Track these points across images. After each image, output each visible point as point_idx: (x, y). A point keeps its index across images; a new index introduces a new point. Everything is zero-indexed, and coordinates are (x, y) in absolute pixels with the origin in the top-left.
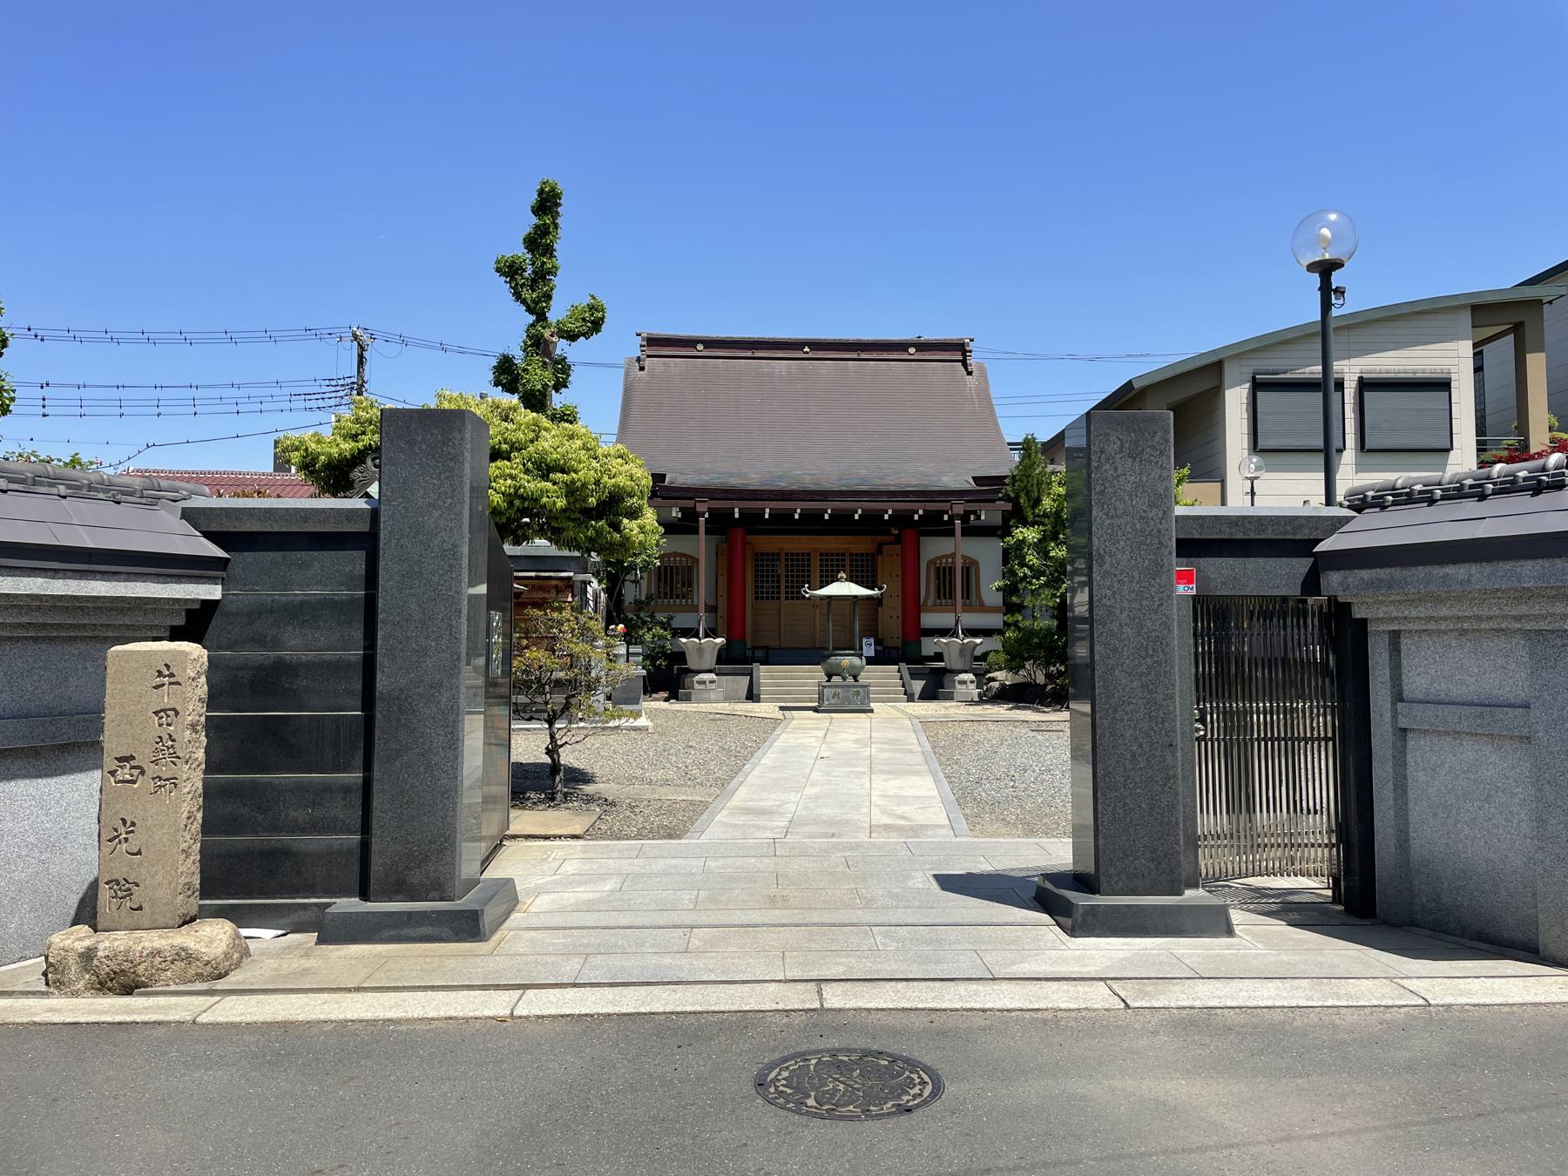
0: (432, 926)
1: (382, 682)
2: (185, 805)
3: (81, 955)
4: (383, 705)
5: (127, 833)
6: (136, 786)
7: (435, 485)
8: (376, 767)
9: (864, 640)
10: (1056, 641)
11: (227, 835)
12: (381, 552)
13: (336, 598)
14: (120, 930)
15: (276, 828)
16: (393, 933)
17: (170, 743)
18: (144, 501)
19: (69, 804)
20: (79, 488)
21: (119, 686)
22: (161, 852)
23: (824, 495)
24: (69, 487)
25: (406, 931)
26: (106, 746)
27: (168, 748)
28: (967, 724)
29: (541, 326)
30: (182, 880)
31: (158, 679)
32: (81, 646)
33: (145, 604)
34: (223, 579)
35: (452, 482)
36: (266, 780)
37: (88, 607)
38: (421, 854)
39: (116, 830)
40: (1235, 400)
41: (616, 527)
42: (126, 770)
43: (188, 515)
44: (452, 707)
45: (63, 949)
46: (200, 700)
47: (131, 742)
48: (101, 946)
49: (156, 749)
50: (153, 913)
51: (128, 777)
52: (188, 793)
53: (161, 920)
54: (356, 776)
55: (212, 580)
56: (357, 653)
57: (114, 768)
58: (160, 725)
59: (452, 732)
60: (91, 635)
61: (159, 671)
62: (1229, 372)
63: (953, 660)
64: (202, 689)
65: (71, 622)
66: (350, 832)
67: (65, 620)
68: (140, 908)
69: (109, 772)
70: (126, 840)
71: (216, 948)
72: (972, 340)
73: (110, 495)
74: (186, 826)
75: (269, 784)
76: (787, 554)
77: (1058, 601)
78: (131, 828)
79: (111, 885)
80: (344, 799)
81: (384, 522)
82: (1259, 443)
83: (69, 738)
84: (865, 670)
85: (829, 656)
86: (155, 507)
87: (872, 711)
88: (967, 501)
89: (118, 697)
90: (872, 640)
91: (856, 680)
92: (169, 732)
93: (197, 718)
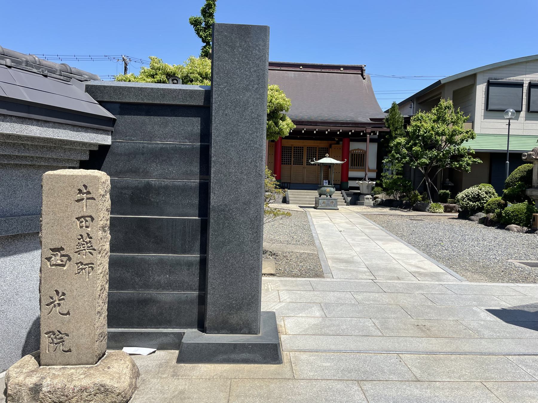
0: (249, 353)
1: (214, 200)
2: (99, 281)
3: (31, 389)
4: (214, 214)
5: (60, 300)
6: (65, 268)
7: (247, 75)
8: (210, 252)
9: (324, 181)
10: (406, 184)
11: (117, 289)
12: (213, 118)
13: (182, 147)
14: (57, 365)
15: (147, 286)
16: (225, 357)
17: (88, 240)
18: (62, 78)
19: (19, 273)
20: (20, 63)
21: (52, 200)
22: (83, 314)
23: (315, 123)
24: (13, 61)
25: (233, 356)
26: (43, 240)
27: (87, 243)
28: (381, 216)
29: (208, 47)
30: (98, 332)
31: (79, 195)
32: (24, 171)
33: (65, 145)
34: (112, 132)
35: (258, 74)
36: (141, 257)
37: (28, 144)
38: (237, 305)
39: (52, 298)
40: (480, 90)
41: (276, 124)
42: (58, 257)
43: (90, 90)
44: (256, 216)
45: (18, 384)
46: (107, 209)
47: (61, 238)
48: (45, 383)
49: (79, 243)
50: (79, 354)
51: (59, 262)
52: (101, 273)
53: (84, 359)
54: (195, 256)
55: (105, 132)
56: (195, 181)
57: (50, 256)
58: (81, 227)
59: (256, 232)
60: (30, 163)
61: (79, 190)
62: (479, 78)
63: (363, 190)
64: (108, 204)
65: (16, 154)
66: (192, 289)
67: (13, 152)
68: (70, 351)
69: (46, 259)
70: (59, 305)
71: (124, 382)
72: (365, 66)
73: (40, 70)
74: (100, 296)
75: (143, 260)
76: (294, 147)
77: (414, 167)
78: (62, 297)
79: (49, 335)
80: (188, 270)
81: (215, 98)
82: (489, 108)
83: (18, 231)
84: (335, 193)
85: (321, 187)
86: (69, 83)
87: (338, 209)
88: (372, 127)
89: (51, 207)
90: (327, 181)
91: (331, 197)
92: (88, 232)
93: (106, 222)
